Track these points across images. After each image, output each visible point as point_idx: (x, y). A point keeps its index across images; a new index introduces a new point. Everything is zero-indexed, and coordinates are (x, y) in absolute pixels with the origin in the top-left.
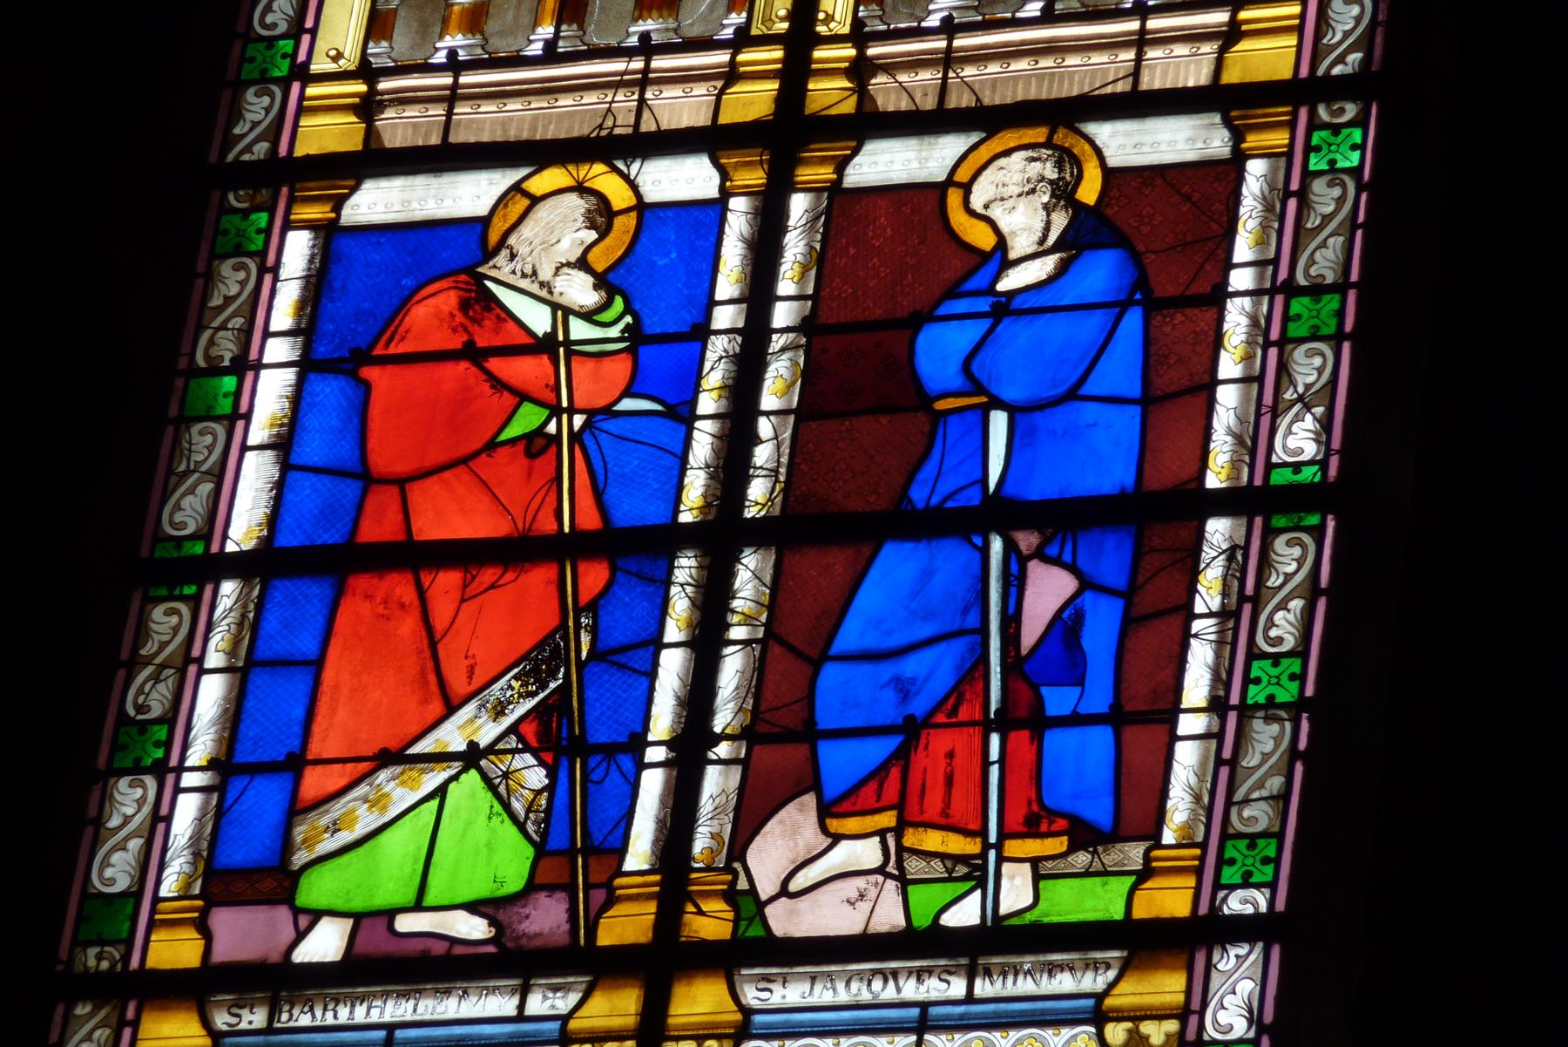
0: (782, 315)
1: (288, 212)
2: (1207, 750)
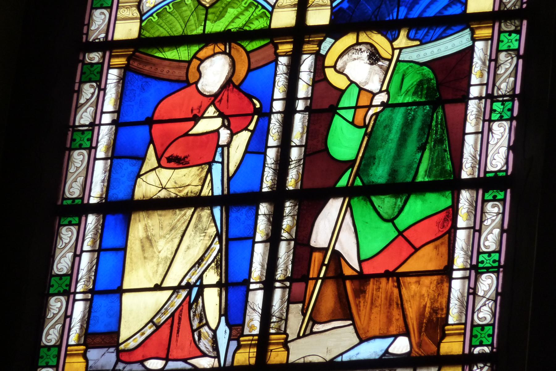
0: (295, 154)
1: (109, 61)
2: (470, 233)
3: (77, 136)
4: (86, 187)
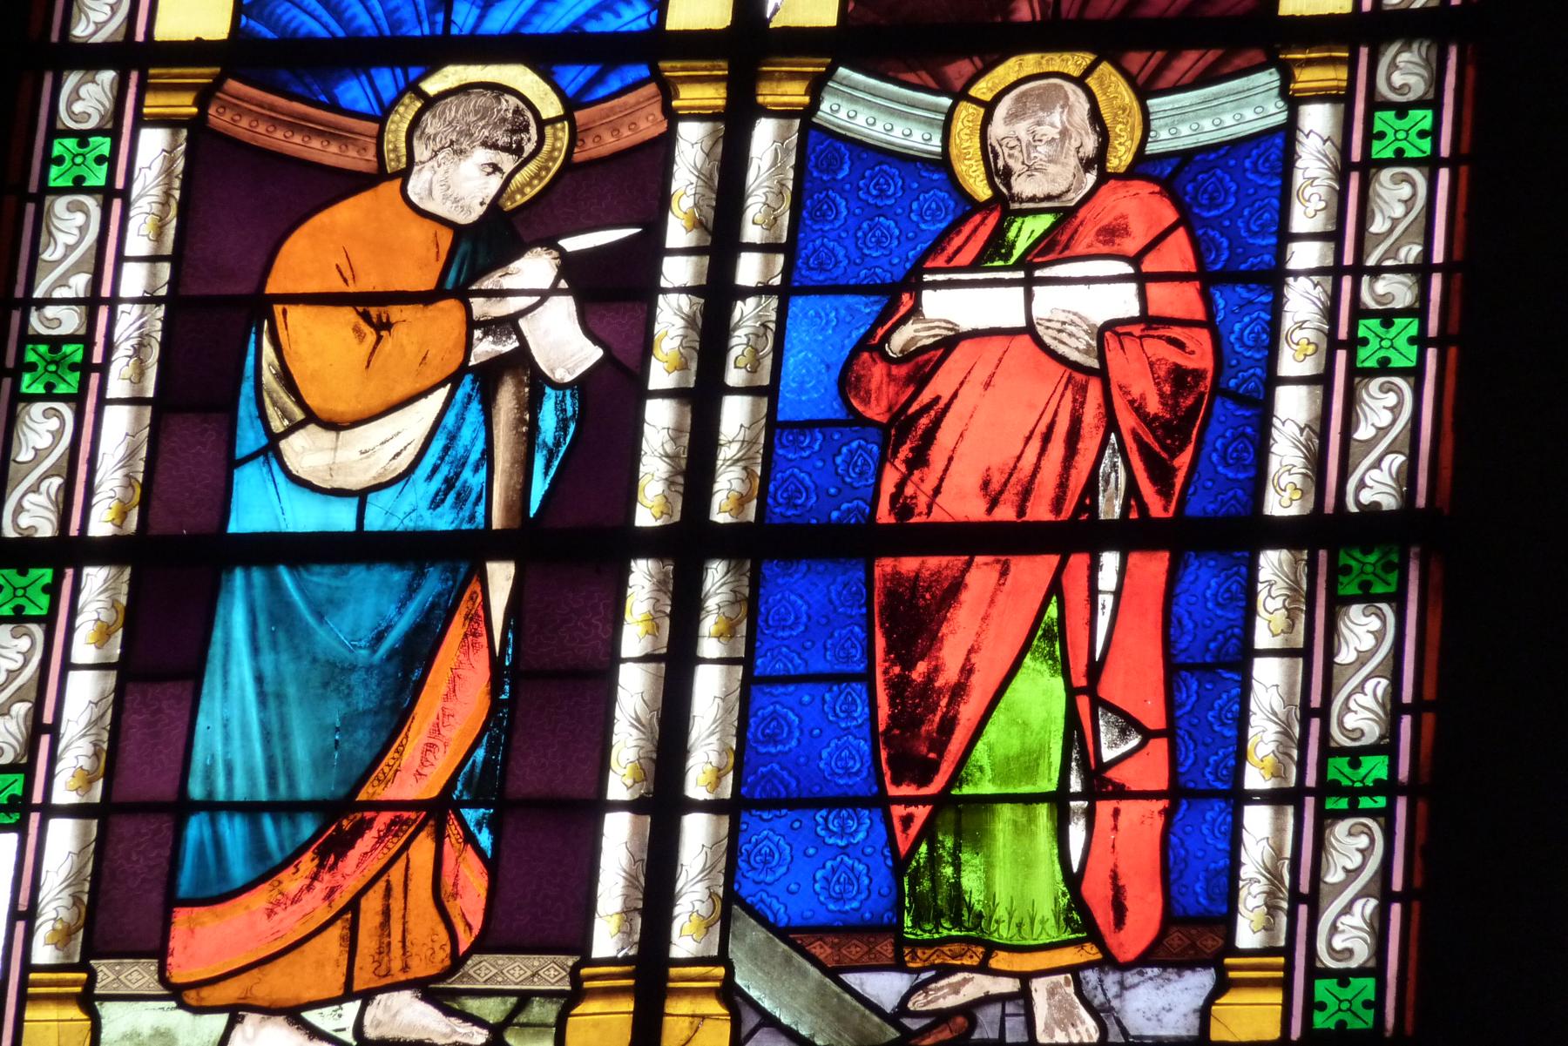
1: (139, 103)
4: (75, 470)
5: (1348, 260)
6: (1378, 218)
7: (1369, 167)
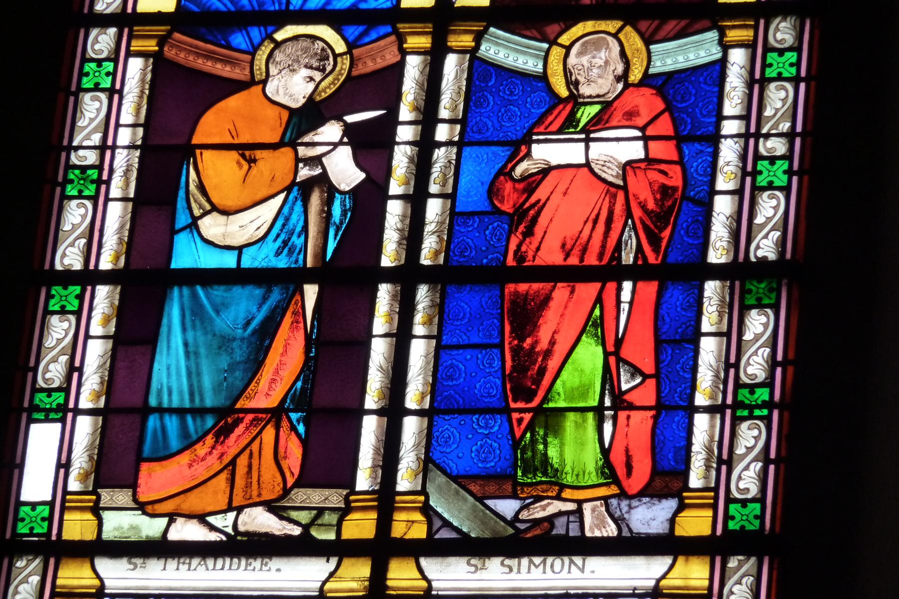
3: (90, 67)
4: (93, 235)
5: (753, 130)
6: (768, 108)
7: (764, 82)
